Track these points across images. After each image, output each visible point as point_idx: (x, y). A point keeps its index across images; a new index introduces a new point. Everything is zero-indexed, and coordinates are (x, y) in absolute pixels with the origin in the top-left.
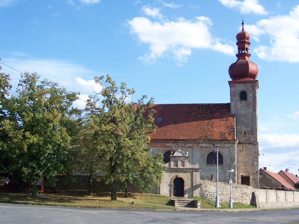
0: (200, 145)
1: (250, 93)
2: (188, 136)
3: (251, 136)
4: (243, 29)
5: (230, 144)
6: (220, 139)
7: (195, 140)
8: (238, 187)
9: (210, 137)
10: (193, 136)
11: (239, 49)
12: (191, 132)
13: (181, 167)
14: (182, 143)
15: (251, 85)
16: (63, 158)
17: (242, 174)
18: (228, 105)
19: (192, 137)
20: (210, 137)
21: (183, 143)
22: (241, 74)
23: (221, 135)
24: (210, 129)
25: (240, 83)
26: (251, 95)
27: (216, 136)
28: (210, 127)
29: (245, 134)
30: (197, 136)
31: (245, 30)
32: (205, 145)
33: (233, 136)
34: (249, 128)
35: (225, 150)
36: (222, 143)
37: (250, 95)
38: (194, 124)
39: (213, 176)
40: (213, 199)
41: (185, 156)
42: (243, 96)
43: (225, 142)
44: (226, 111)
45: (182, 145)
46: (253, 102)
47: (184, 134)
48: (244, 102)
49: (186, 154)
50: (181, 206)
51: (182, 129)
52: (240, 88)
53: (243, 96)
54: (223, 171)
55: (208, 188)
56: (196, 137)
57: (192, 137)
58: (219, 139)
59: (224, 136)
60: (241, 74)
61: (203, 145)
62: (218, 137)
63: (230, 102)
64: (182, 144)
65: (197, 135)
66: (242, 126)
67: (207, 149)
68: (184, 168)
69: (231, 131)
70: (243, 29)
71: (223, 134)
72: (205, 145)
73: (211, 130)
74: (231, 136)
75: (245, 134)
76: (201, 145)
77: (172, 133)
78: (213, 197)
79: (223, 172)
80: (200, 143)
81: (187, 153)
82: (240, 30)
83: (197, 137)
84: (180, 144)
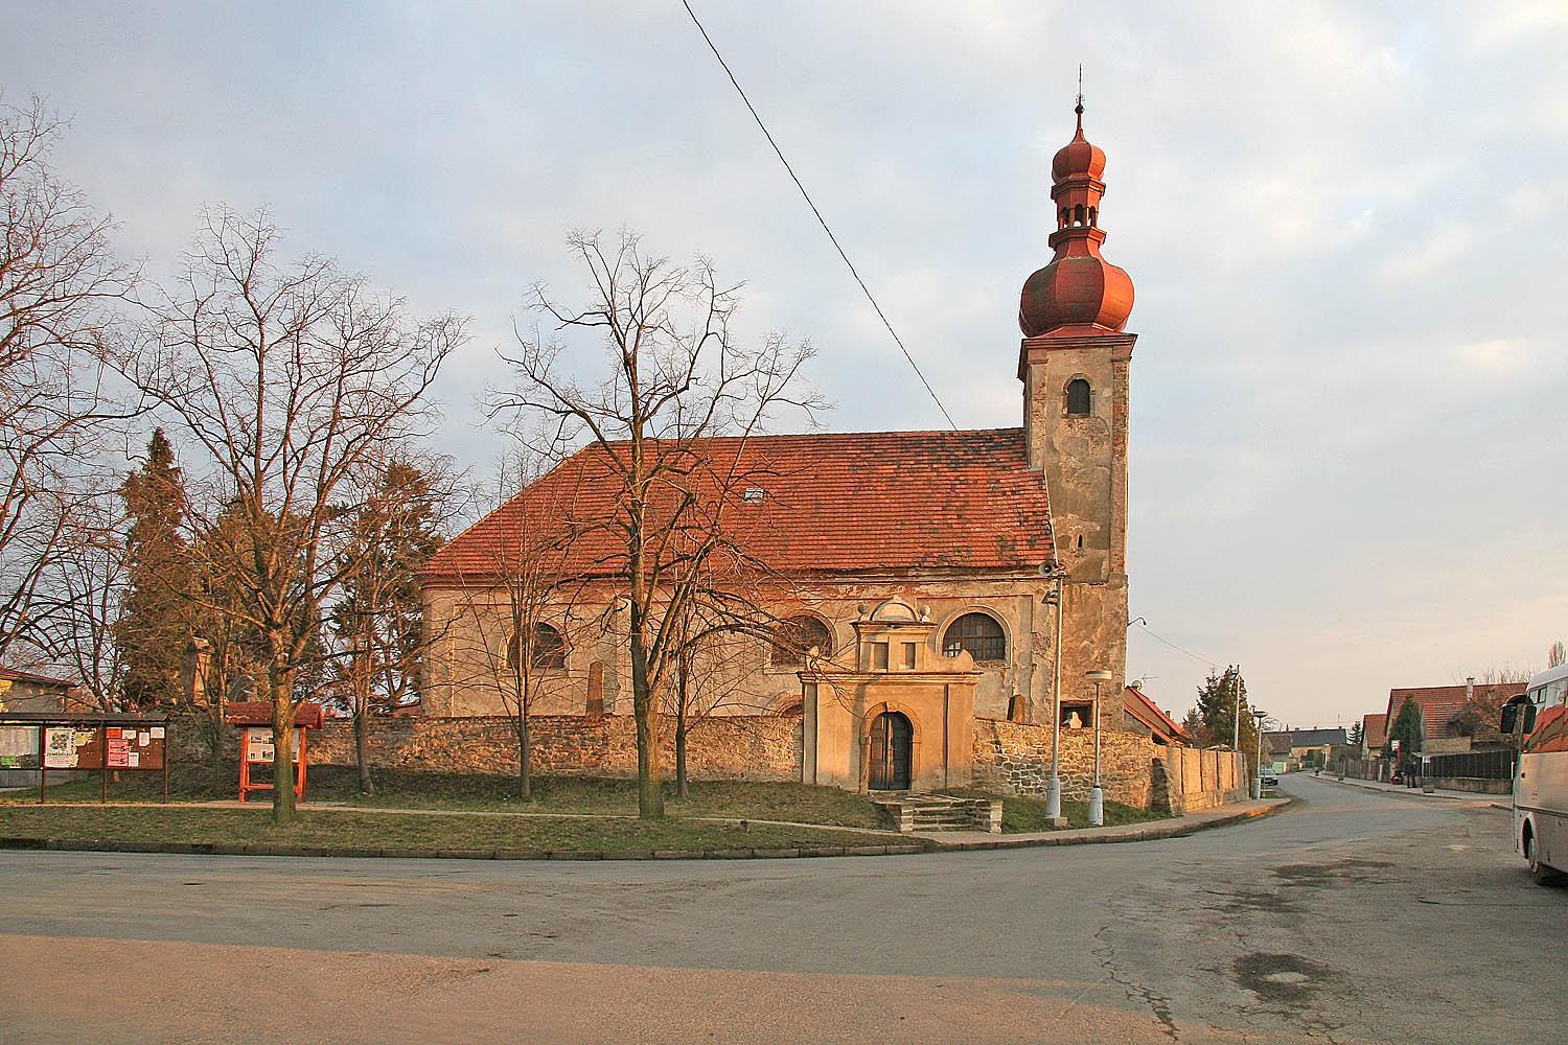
0: (917, 589)
1: (1105, 386)
2: (872, 556)
3: (1103, 553)
4: (1079, 130)
5: (1035, 584)
6: (999, 563)
7: (900, 572)
8: (1108, 742)
9: (958, 558)
10: (892, 555)
11: (1063, 214)
12: (883, 541)
13: (903, 668)
14: (849, 583)
15: (1105, 353)
16: (223, 847)
17: (1065, 698)
18: (1015, 441)
19: (889, 560)
20: (958, 558)
21: (853, 583)
22: (1071, 308)
23: (999, 549)
24: (954, 526)
25: (1067, 345)
26: (1107, 392)
27: (982, 554)
28: (952, 519)
29: (1080, 545)
30: (906, 555)
31: (1088, 137)
32: (939, 590)
33: (1046, 552)
34: (1094, 524)
35: (1014, 607)
36: (1003, 580)
37: (1102, 396)
38: (892, 510)
39: (1017, 701)
40: (1022, 792)
41: (918, 619)
42: (1079, 397)
43: (1016, 576)
44: (1011, 459)
45: (847, 592)
46: (1115, 420)
47: (854, 547)
48: (1080, 422)
49: (923, 613)
50: (923, 829)
51: (845, 528)
52: (1062, 365)
53: (1079, 397)
54: (1003, 687)
55: (1003, 751)
56: (903, 560)
57: (889, 560)
58: (994, 564)
59: (1012, 553)
60: (1071, 308)
61: (932, 589)
62: (991, 558)
63: (1021, 425)
64: (848, 587)
65: (906, 550)
66: (1070, 516)
67: (947, 604)
68: (913, 671)
69: (1035, 533)
70: (1079, 130)
71: (1009, 543)
72: (939, 590)
73: (960, 531)
74: (1040, 552)
75: (1080, 545)
76: (923, 588)
77: (810, 547)
78: (1021, 785)
79: (1003, 691)
80: (918, 584)
81: (928, 610)
82: (1066, 139)
83: (910, 560)
84: (842, 589)
